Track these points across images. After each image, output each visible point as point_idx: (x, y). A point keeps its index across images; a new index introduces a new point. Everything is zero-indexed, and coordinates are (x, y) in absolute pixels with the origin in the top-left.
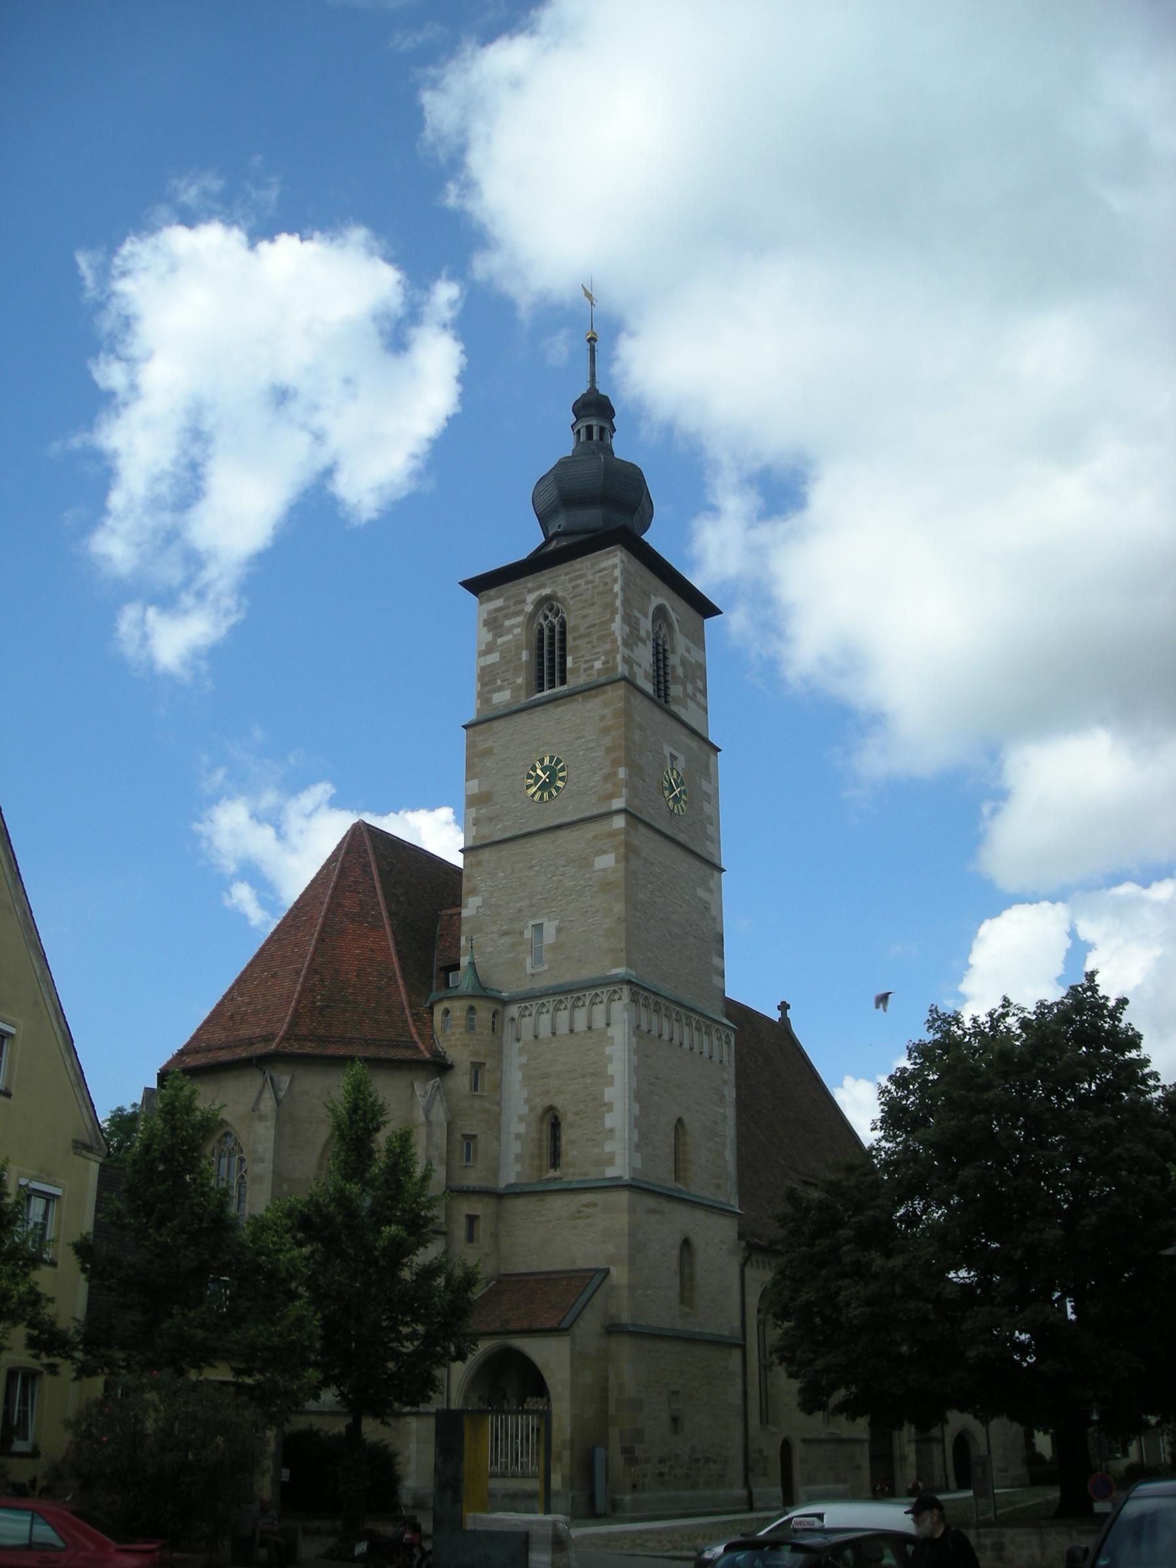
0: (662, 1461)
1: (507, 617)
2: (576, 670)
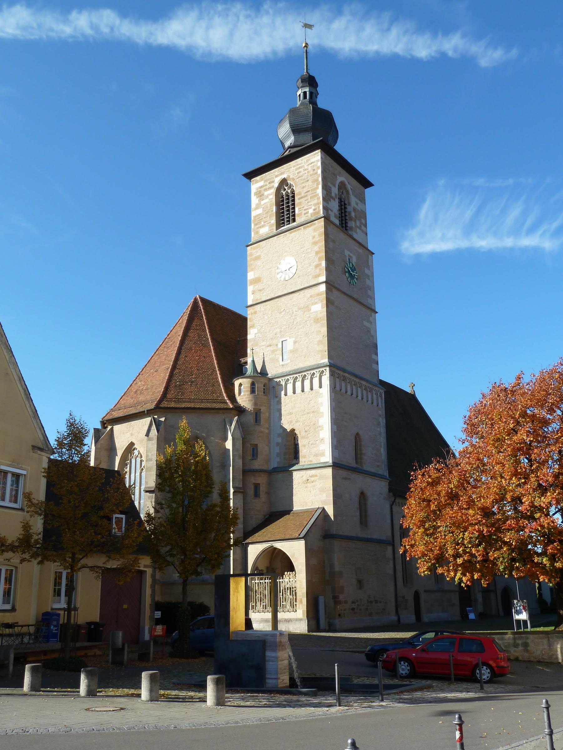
0: (353, 602)
1: (266, 190)
2: (300, 215)
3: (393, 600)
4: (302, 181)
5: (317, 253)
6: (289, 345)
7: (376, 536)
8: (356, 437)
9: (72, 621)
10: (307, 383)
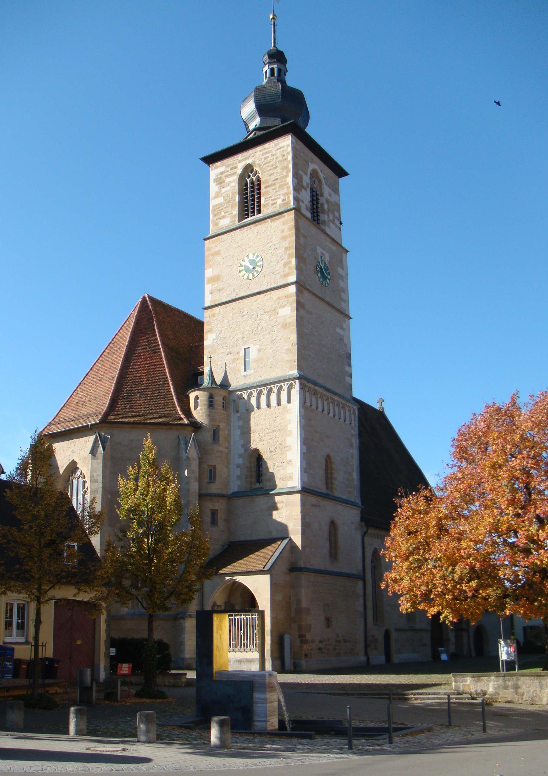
1: (227, 176)
2: (266, 205)
3: (362, 639)
4: (270, 168)
5: (286, 249)
6: (253, 354)
7: (345, 570)
8: (326, 459)
9: (40, 656)
10: (273, 397)
